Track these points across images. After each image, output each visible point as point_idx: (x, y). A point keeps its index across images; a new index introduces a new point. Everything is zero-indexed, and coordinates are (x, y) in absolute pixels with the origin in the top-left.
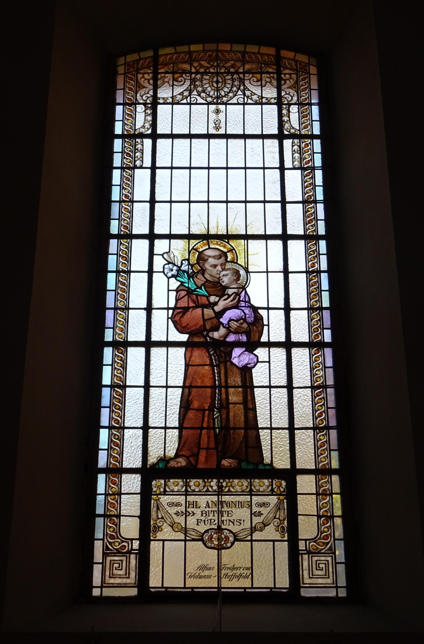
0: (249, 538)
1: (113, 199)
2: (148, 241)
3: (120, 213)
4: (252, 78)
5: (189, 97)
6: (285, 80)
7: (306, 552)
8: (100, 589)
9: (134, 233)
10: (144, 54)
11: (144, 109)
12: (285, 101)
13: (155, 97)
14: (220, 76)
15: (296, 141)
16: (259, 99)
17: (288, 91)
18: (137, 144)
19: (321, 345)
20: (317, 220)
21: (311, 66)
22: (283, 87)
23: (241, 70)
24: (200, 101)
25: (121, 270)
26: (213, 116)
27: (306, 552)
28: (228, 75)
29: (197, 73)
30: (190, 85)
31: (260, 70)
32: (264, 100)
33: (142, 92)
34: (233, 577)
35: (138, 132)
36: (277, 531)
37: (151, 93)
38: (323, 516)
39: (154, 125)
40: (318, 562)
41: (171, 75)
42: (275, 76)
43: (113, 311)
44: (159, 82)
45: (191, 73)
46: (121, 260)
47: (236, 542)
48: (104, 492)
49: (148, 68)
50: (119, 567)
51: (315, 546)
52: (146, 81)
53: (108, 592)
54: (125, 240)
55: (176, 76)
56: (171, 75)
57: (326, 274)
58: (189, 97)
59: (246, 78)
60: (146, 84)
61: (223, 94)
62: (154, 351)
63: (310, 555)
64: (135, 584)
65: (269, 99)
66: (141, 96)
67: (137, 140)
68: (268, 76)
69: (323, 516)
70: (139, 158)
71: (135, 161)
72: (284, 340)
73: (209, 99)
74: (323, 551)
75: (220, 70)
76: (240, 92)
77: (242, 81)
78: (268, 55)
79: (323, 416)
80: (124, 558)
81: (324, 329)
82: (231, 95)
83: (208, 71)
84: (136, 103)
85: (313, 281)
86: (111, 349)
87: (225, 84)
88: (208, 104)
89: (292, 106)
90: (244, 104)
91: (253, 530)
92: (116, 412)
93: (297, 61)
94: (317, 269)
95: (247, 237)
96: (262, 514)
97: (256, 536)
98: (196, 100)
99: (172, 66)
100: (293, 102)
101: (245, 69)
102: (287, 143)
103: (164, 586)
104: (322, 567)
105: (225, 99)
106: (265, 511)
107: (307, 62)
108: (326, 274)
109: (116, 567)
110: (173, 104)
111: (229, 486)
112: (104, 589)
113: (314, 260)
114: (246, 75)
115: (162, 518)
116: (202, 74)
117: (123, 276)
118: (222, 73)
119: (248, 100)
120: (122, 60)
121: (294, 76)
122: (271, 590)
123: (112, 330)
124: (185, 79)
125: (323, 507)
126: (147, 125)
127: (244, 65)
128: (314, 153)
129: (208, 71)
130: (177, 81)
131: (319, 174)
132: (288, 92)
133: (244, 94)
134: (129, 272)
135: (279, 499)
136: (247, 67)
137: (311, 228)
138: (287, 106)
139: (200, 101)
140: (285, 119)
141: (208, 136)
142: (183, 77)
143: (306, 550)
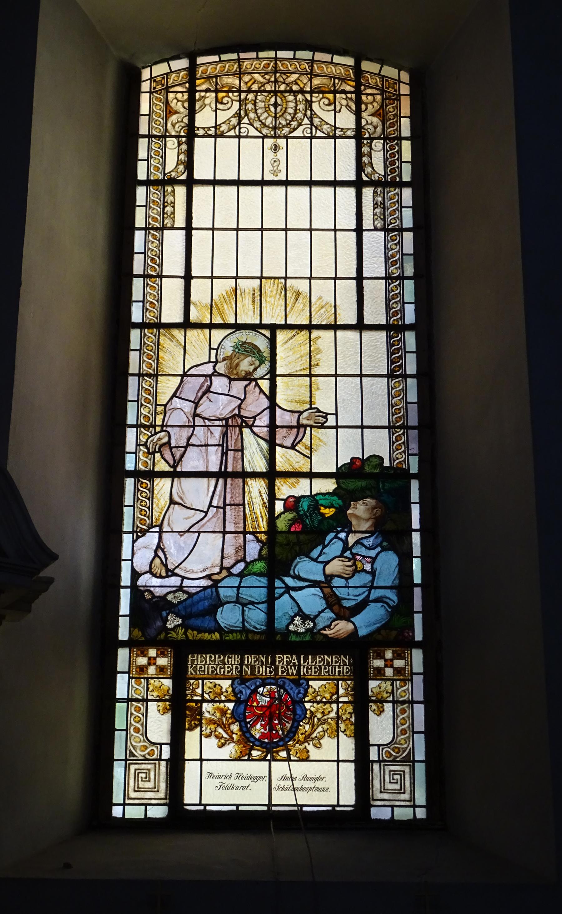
1: (129, 422)
4: (321, 99)
5: (237, 128)
6: (366, 105)
8: (122, 807)
11: (176, 144)
14: (279, 97)
15: (379, 190)
17: (370, 119)
18: (166, 204)
22: (364, 115)
25: (144, 373)
26: (268, 155)
29: (249, 91)
30: (240, 110)
32: (338, 133)
33: (174, 118)
35: (169, 177)
37: (186, 120)
39: (189, 166)
42: (353, 95)
44: (197, 107)
45: (240, 91)
46: (144, 394)
48: (148, 90)
50: (146, 778)
52: (180, 104)
55: (221, 95)
56: (213, 95)
58: (237, 128)
59: (314, 99)
60: (178, 107)
61: (284, 122)
63: (382, 764)
67: (166, 188)
68: (344, 96)
70: (169, 214)
73: (265, 131)
74: (398, 759)
76: (306, 121)
82: (294, 124)
88: (264, 137)
89: (375, 141)
90: (311, 138)
93: (383, 77)
94: (398, 225)
99: (214, 80)
100: (376, 135)
101: (313, 85)
102: (368, 193)
104: (397, 779)
105: (286, 131)
108: (412, 282)
110: (216, 136)
117: (147, 381)
118: (281, 92)
122: (334, 809)
123: (134, 455)
124: (232, 101)
125: (395, 386)
127: (310, 80)
130: (222, 103)
136: (316, 82)
138: (369, 141)
140: (365, 159)
142: (229, 97)
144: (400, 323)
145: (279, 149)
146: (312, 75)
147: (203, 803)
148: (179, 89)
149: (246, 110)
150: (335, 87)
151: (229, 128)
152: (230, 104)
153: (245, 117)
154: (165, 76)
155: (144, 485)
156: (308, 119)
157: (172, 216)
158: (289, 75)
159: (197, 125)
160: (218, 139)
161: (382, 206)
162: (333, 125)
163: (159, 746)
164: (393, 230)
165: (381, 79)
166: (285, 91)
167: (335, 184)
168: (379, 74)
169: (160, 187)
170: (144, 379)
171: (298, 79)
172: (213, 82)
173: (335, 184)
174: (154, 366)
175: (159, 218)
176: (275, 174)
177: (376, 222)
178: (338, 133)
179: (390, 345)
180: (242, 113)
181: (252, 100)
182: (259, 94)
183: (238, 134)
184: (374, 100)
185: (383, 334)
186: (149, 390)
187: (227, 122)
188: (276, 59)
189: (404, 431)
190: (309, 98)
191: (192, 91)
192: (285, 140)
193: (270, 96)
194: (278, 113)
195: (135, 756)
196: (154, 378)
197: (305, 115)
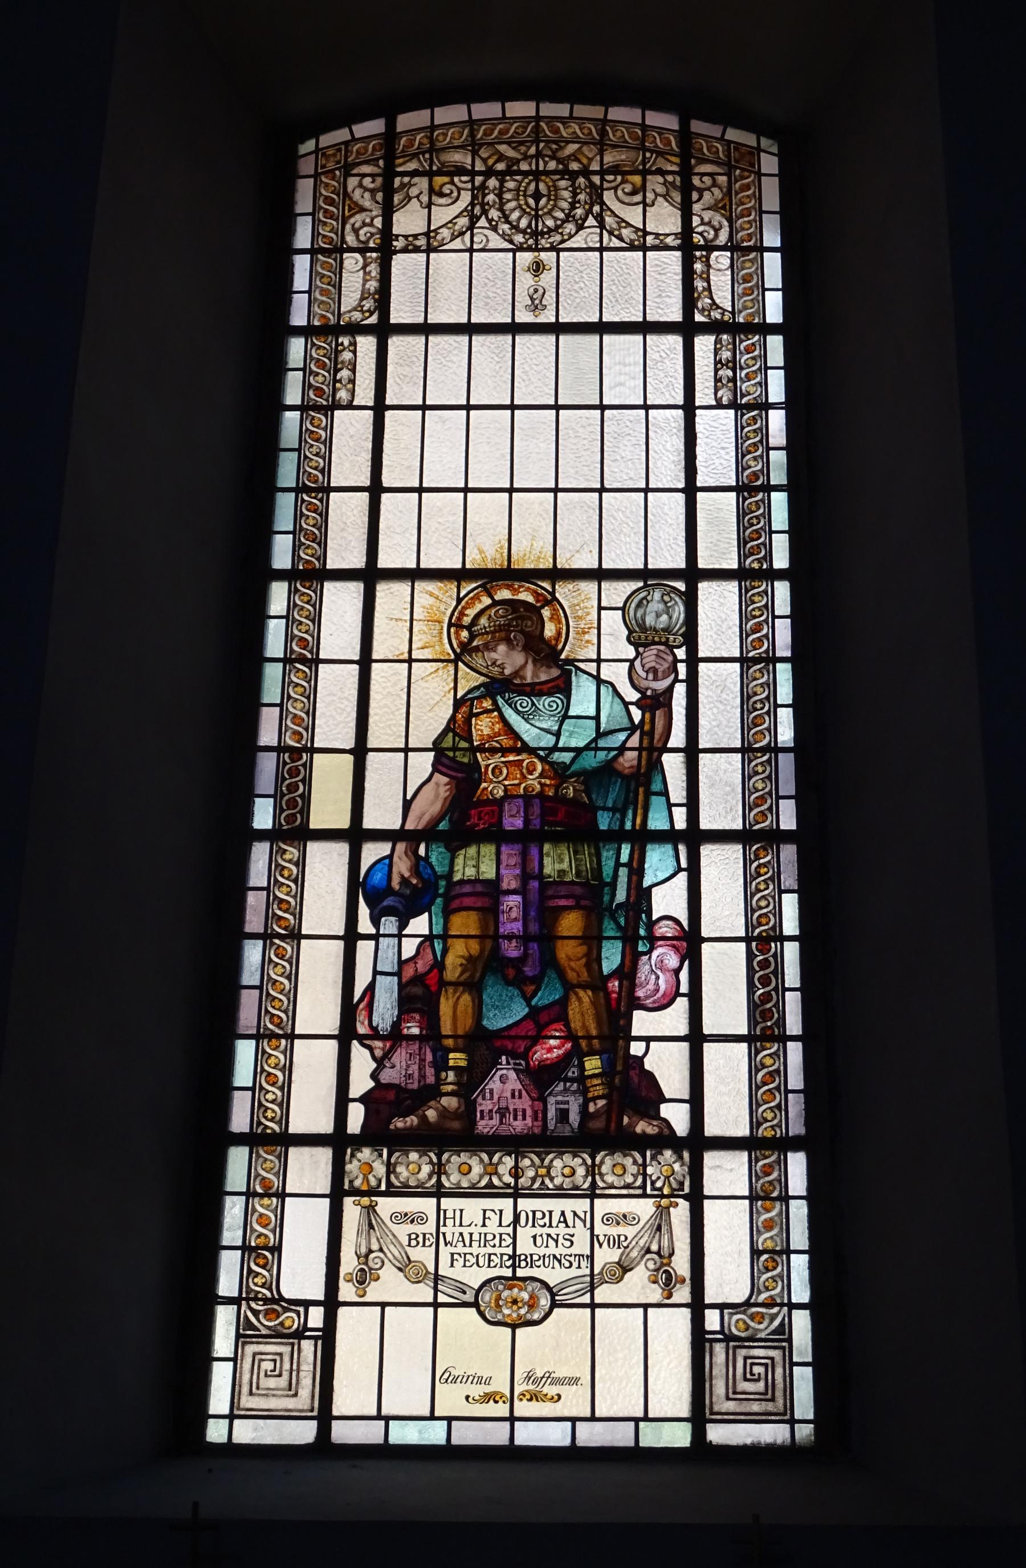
0: (586, 1299)
2: (375, 340)
3: (298, 516)
6: (701, 191)
9: (292, 1130)
10: (362, 129)
13: (387, 232)
16: (639, 237)
17: (707, 216)
18: (340, 348)
19: (774, 837)
20: (771, 532)
21: (762, 154)
22: (696, 208)
23: (595, 166)
26: (526, 281)
28: (562, 179)
29: (489, 173)
30: (472, 204)
32: (650, 240)
33: (358, 219)
34: (544, 1380)
37: (378, 222)
40: (749, 1361)
43: (281, 664)
44: (396, 199)
45: (473, 173)
47: (667, 1096)
51: (745, 1322)
52: (367, 195)
53: (246, 1433)
55: (439, 180)
57: (788, 666)
59: (606, 185)
62: (384, 591)
64: (312, 1410)
65: (661, 237)
67: (340, 340)
68: (661, 179)
71: (335, 391)
72: (683, 565)
74: (762, 1335)
76: (591, 221)
77: (596, 195)
79: (765, 632)
80: (286, 1350)
81: (779, 797)
82: (570, 227)
83: (515, 168)
84: (339, 249)
85: (745, 271)
87: (555, 206)
89: (716, 254)
90: (601, 250)
92: (304, 594)
93: (730, 142)
97: (602, 1294)
98: (485, 241)
99: (427, 156)
102: (704, 344)
104: (759, 1374)
107: (755, 144)
109: (266, 1371)
111: (542, 1167)
112: (236, 1422)
113: (756, 451)
116: (501, 176)
117: (299, 670)
118: (547, 173)
119: (610, 240)
120: (309, 145)
121: (722, 180)
124: (459, 190)
126: (368, 304)
127: (601, 153)
128: (767, 368)
130: (442, 195)
131: (777, 420)
132: (706, 220)
133: (602, 225)
134: (315, 662)
135: (658, 1206)
136: (609, 158)
137: (752, 435)
140: (699, 284)
141: (514, 329)
143: (722, 1331)
144: (765, 567)
145: (544, 269)
148: (366, 169)
149: (483, 205)
152: (455, 194)
154: (343, 147)
155: (325, 280)
156: (595, 218)
158: (563, 144)
159: (395, 231)
164: (750, 407)
165: (726, 148)
167: (645, 328)
170: (272, 944)
173: (645, 328)
177: (719, 394)
179: (741, 514)
180: (477, 210)
181: (495, 188)
182: (508, 178)
183: (469, 245)
184: (715, 184)
188: (538, 118)
189: (771, 756)
190: (598, 182)
191: (389, 174)
194: (542, 209)
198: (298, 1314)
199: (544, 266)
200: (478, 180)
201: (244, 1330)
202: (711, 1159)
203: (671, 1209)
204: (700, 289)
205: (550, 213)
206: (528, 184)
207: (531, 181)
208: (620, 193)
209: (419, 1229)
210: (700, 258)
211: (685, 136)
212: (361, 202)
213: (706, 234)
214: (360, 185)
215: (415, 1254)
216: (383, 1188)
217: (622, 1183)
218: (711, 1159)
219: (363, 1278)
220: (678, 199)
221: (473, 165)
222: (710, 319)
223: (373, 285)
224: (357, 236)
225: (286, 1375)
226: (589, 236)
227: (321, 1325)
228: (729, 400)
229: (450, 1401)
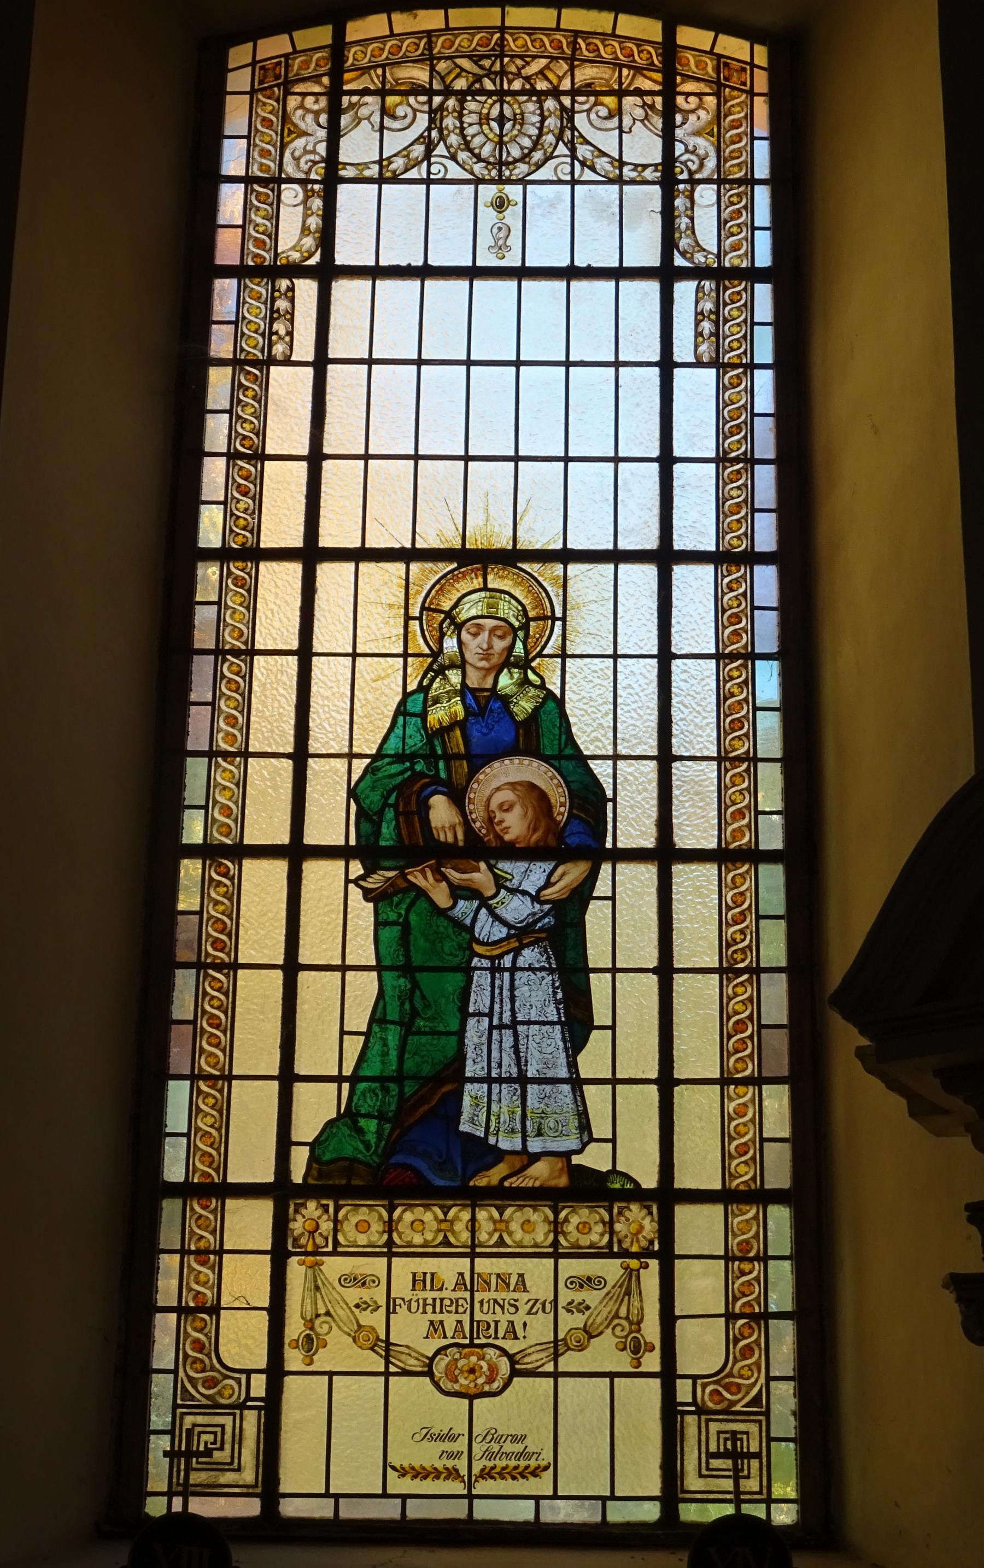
0: (550, 1368)
6: (686, 113)
7: (693, 1408)
11: (301, 196)
12: (682, 172)
14: (508, 103)
15: (708, 285)
17: (692, 141)
22: (679, 133)
23: (566, 85)
24: (455, 171)
25: (227, 647)
27: (693, 1408)
30: (429, 129)
31: (616, 87)
36: (622, 1350)
37: (322, 149)
38: (742, 1316)
39: (327, 238)
41: (378, 99)
42: (659, 100)
47: (515, 1379)
49: (316, 79)
52: (310, 118)
54: (240, 564)
55: (390, 100)
60: (308, 123)
63: (703, 1418)
66: (294, 158)
68: (638, 100)
69: (742, 1316)
74: (738, 1408)
75: (510, 82)
76: (562, 149)
78: (639, 42)
84: (276, 181)
86: (198, 864)
88: (478, 181)
90: (573, 182)
91: (557, 1348)
93: (719, 56)
95: (566, 556)
96: (588, 1308)
97: (568, 1362)
99: (379, 71)
101: (576, 81)
102: (684, 291)
103: (331, 1492)
105: (522, 169)
106: (592, 1297)
108: (775, 665)
110: (380, 180)
114: (581, 99)
115: (328, 1314)
116: (462, 96)
120: (239, 55)
121: (711, 101)
124: (415, 111)
126: (309, 242)
127: (572, 69)
129: (477, 86)
130: (394, 117)
132: (691, 148)
136: (585, 74)
139: (455, 171)
140: (683, 222)
141: (473, 273)
142: (410, 105)
143: (694, 1403)
146: (573, 61)
147: (332, 1500)
150: (621, 84)
151: (406, 165)
153: (439, 143)
154: (283, 59)
156: (565, 144)
157: (290, 294)
158: (528, 59)
159: (342, 158)
160: (384, 186)
161: (713, 317)
162: (617, 157)
163: (243, 1378)
166: (522, 92)
168: (711, 52)
169: (214, 1201)
170: (206, 975)
171: (547, 67)
172: (378, 77)
174: (235, 830)
175: (274, 119)
176: (500, 255)
178: (628, 173)
180: (434, 134)
182: (469, 98)
183: (425, 177)
185: (709, 569)
186: (210, 1155)
187: (405, 153)
191: (335, 94)
192: (521, 187)
193: (490, 101)
195: (193, 1398)
196: (229, 973)
197: (559, 138)
198: (239, 1382)
199: (509, 201)
200: (437, 100)
201: (182, 1400)
202: (683, 1214)
203: (642, 1271)
204: (683, 227)
205: (513, 139)
206: (492, 105)
207: (495, 102)
208: (593, 116)
209: (364, 1294)
210: (683, 193)
211: (669, 49)
212: (302, 126)
213: (689, 164)
214: (301, 106)
215: (366, 1318)
216: (330, 1248)
217: (588, 1243)
218: (683, 1214)
219: (310, 1343)
220: (659, 124)
221: (431, 83)
222: (693, 263)
223: (314, 222)
224: (298, 165)
225: (228, 1447)
226: (559, 166)
227: (263, 1394)
228: (711, 357)
229: (397, 1485)
